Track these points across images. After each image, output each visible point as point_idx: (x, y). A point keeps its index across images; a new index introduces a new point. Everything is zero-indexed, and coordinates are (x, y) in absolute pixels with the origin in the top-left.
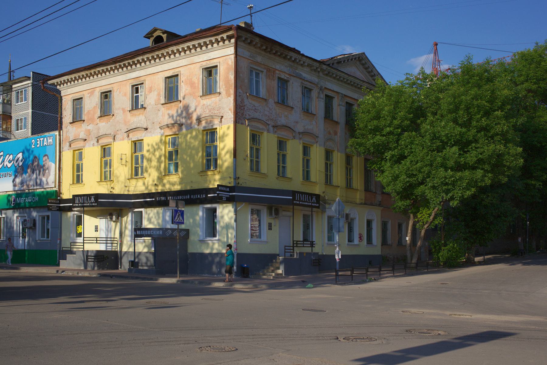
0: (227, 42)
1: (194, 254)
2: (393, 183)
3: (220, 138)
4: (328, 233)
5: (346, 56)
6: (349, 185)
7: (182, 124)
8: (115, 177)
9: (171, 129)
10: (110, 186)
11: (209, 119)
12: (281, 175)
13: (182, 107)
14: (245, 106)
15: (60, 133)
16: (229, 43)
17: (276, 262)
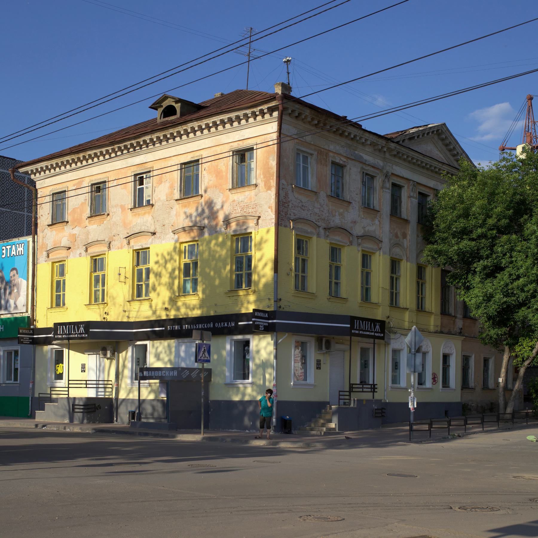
0: (267, 116)
1: (218, 403)
2: (484, 304)
3: (255, 245)
4: (392, 372)
5: (420, 129)
6: (420, 307)
7: (204, 227)
8: (110, 297)
9: (189, 233)
10: (104, 310)
11: (242, 222)
12: (333, 295)
13: (203, 204)
14: (289, 202)
15: (34, 238)
16: (270, 117)
17: (327, 413)
